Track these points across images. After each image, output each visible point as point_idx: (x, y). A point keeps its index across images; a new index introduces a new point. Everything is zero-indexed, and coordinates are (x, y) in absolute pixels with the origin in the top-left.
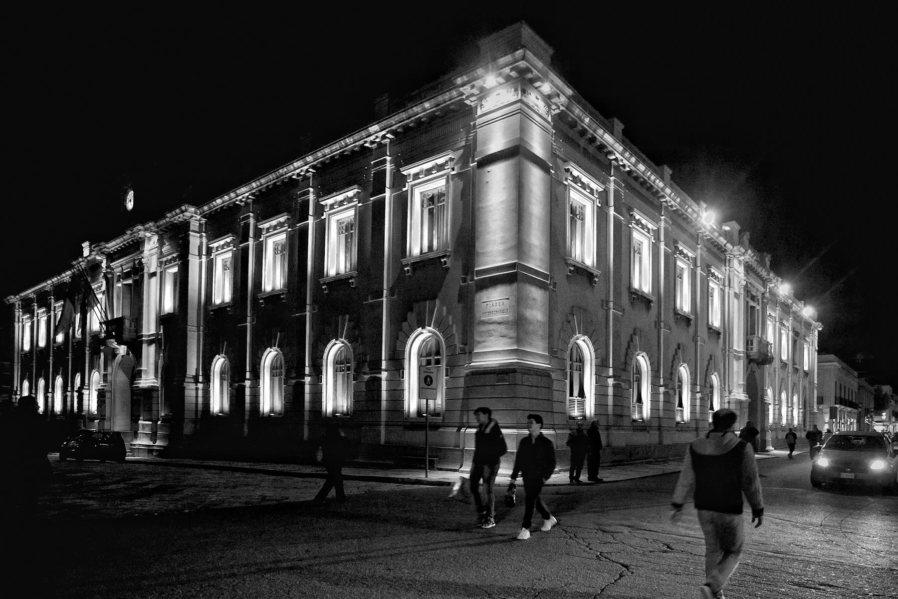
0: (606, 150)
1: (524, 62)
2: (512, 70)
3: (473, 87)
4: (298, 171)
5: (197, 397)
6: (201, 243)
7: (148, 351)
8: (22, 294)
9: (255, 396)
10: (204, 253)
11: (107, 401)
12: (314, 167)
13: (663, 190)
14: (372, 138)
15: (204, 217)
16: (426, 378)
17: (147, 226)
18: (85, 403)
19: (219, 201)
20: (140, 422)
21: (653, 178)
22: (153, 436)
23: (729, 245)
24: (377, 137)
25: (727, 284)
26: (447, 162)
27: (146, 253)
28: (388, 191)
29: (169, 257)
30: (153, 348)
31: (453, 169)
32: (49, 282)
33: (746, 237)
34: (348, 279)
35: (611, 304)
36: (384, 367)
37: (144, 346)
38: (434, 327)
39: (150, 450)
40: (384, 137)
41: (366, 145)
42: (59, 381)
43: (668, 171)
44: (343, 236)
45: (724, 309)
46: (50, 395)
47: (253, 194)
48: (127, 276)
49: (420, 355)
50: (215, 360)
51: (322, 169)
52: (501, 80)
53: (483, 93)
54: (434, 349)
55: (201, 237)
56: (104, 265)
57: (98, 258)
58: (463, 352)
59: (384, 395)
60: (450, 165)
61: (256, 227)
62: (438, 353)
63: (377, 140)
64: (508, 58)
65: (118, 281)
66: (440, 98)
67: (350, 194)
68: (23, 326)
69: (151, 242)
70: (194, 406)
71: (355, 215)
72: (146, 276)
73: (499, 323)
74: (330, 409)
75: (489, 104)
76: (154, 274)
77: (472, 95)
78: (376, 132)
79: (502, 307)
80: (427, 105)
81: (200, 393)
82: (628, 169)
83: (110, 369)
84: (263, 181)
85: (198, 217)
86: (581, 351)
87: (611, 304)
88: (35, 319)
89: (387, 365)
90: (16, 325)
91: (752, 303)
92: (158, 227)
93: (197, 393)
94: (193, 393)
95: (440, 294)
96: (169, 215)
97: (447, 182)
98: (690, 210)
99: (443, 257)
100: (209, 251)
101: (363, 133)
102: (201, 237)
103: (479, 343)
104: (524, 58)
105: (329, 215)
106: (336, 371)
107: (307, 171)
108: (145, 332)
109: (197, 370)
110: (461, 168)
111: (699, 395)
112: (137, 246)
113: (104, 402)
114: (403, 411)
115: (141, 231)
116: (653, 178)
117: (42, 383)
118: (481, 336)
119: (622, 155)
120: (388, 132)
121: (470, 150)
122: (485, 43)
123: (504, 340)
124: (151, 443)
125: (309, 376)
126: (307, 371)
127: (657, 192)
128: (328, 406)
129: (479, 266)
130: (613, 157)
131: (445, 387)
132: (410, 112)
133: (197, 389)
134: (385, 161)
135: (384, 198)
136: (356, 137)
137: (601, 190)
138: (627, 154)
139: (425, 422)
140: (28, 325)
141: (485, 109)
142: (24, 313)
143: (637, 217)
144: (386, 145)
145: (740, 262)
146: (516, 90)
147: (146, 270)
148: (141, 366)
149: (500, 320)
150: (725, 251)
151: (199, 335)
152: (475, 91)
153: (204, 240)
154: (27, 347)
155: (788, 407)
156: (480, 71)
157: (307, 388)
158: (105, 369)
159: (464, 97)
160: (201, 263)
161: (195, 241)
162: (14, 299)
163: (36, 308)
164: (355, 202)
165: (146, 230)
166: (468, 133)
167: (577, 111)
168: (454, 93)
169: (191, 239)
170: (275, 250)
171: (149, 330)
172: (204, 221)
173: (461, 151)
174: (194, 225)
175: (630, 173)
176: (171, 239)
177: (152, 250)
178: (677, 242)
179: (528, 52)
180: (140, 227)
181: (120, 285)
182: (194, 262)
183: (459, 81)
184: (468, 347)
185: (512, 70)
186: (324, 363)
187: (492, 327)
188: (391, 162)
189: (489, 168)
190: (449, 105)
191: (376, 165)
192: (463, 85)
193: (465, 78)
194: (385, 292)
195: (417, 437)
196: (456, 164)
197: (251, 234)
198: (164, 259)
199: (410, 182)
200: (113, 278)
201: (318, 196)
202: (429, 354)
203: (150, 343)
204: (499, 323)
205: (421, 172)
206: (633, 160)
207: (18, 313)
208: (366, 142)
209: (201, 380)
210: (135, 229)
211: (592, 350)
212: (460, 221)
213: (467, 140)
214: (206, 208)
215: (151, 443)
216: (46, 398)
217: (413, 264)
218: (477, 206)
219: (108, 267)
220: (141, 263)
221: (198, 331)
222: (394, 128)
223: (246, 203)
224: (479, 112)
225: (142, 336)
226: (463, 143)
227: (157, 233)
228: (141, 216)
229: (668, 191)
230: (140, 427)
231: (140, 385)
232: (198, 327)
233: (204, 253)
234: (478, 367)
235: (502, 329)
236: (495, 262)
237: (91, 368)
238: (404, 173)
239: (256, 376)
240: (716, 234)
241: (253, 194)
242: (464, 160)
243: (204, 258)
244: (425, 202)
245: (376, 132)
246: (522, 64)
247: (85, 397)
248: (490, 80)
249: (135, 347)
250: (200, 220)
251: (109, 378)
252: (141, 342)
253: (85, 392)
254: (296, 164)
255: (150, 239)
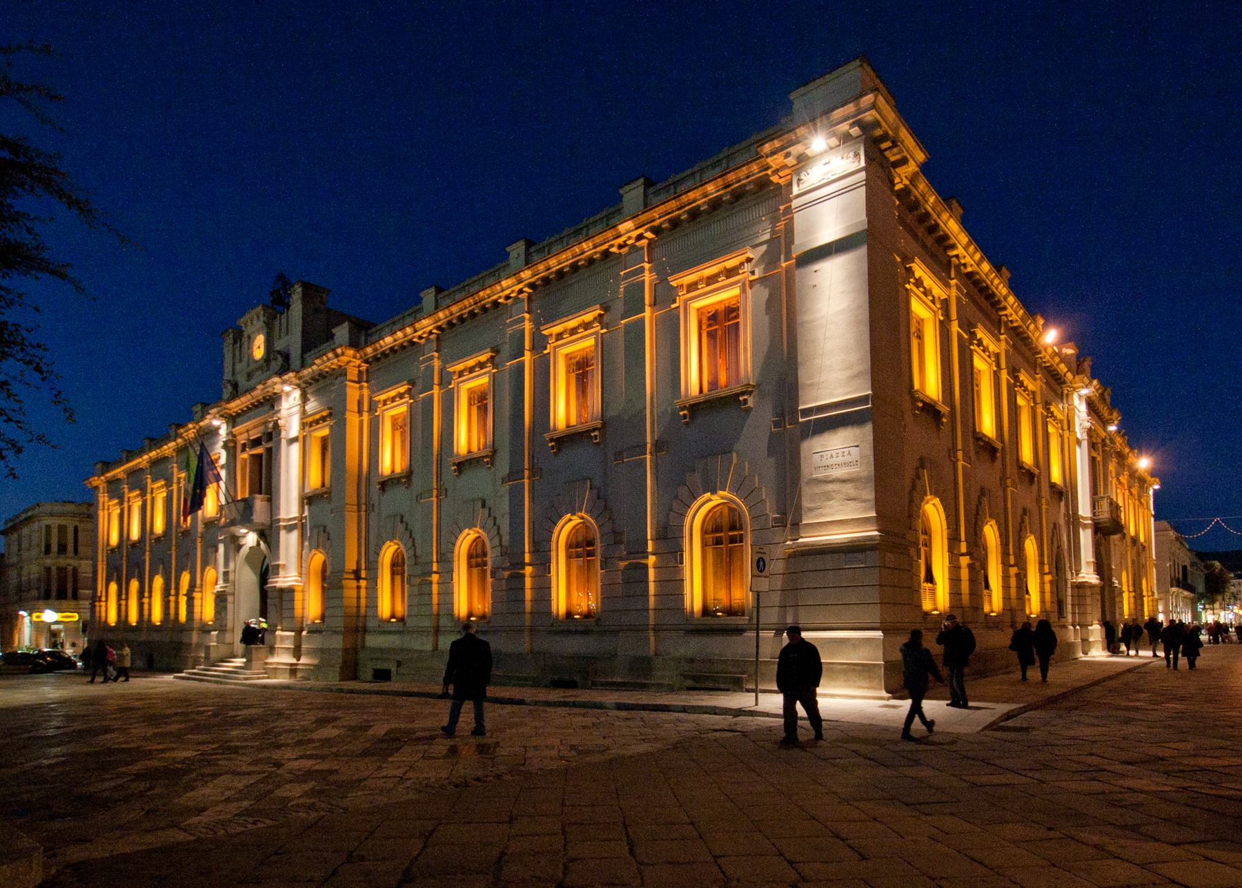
0: (946, 243)
1: (873, 112)
2: (852, 125)
3: (788, 155)
4: (507, 292)
5: (358, 598)
6: (362, 396)
7: (287, 539)
8: (108, 475)
9: (543, 591)
10: (366, 407)
11: (230, 606)
12: (532, 286)
13: (1005, 298)
14: (620, 241)
15: (366, 361)
16: (758, 562)
17: (286, 377)
18: (197, 609)
19: (388, 340)
20: (278, 633)
21: (996, 281)
22: (297, 652)
23: (1069, 375)
24: (630, 238)
25: (1066, 427)
26: (742, 264)
27: (284, 413)
28: (648, 309)
29: (317, 417)
30: (294, 536)
31: (753, 273)
32: (146, 457)
33: (1087, 365)
34: (589, 431)
35: (960, 454)
36: (650, 549)
37: (283, 533)
38: (586, 512)
39: (293, 670)
40: (640, 237)
41: (614, 250)
42: (158, 582)
43: (1006, 273)
44: (573, 376)
45: (1071, 464)
46: (123, 602)
47: (439, 328)
48: (256, 442)
49: (704, 532)
50: (384, 548)
51: (543, 286)
52: (834, 141)
53: (803, 161)
54: (479, 551)
55: (361, 388)
56: (223, 431)
57: (216, 423)
58: (781, 523)
59: (528, 594)
60: (747, 267)
61: (442, 370)
62: (485, 555)
63: (629, 242)
64: (850, 108)
65: (243, 450)
66: (731, 177)
67: (588, 317)
68: (109, 515)
69: (291, 399)
70: (354, 610)
71: (596, 345)
72: (284, 442)
73: (844, 481)
74: (562, 609)
75: (813, 176)
76: (295, 440)
77: (785, 167)
78: (628, 232)
79: (847, 459)
80: (710, 188)
81: (363, 593)
82: (970, 269)
83: (232, 565)
84: (454, 309)
85: (358, 362)
86: (928, 519)
87: (960, 454)
88: (126, 505)
89: (531, 559)
90: (101, 513)
91: (1094, 454)
92: (300, 379)
93: (358, 593)
94: (354, 593)
95: (738, 446)
96: (318, 361)
97: (743, 291)
98: (1032, 326)
99: (743, 393)
100: (372, 409)
101: (609, 234)
102: (361, 388)
103: (811, 510)
104: (874, 106)
105: (555, 348)
106: (569, 557)
107: (521, 291)
108: (283, 515)
109: (358, 562)
110: (766, 270)
111: (1048, 578)
112: (272, 402)
113: (225, 608)
114: (683, 609)
115: (278, 385)
116: (996, 281)
117: (134, 585)
118: (813, 500)
119: (966, 253)
120: (646, 230)
121: (783, 240)
122: (818, 91)
123: (852, 504)
124: (294, 661)
125: (529, 565)
126: (527, 558)
127: (999, 302)
128: (560, 603)
129: (804, 403)
130: (955, 253)
131: (600, 584)
132: (684, 198)
133: (359, 588)
134: (642, 270)
135: (643, 319)
136: (598, 240)
137: (944, 296)
138: (972, 249)
139: (718, 623)
140: (116, 512)
141: (805, 186)
142: (111, 498)
143: (980, 335)
144: (642, 248)
145: (1080, 396)
146: (857, 155)
147: (283, 434)
148: (278, 558)
149: (846, 477)
150: (1064, 382)
151: (359, 518)
152: (791, 161)
153: (366, 392)
154: (114, 539)
155: (1005, 564)
156: (801, 131)
157: (528, 582)
158: (226, 564)
159: (769, 172)
160: (361, 422)
161: (353, 393)
162: (99, 481)
163: (126, 490)
164: (597, 327)
165: (284, 382)
166: (775, 220)
167: (922, 185)
168: (755, 168)
169: (349, 391)
170: (470, 399)
171: (288, 512)
172: (364, 367)
173: (764, 247)
174: (352, 373)
175: (970, 275)
176: (317, 393)
177: (292, 408)
178: (1019, 371)
179: (880, 97)
180: (276, 379)
181: (245, 456)
182: (352, 419)
183: (767, 148)
184: (790, 514)
185: (852, 125)
186: (456, 559)
187: (830, 487)
188: (650, 271)
189: (816, 267)
190: (745, 185)
191: (627, 276)
192: (773, 153)
193: (777, 144)
194: (649, 446)
195: (715, 646)
196: (756, 265)
197: (436, 381)
198: (310, 419)
199: (683, 296)
200: (235, 447)
201: (538, 324)
202: (718, 529)
203: (290, 529)
204: (844, 481)
205: (701, 280)
206: (978, 256)
207: (103, 498)
208: (612, 246)
209: (363, 575)
210: (269, 382)
211: (943, 517)
212: (766, 341)
213: (773, 232)
214: (369, 350)
215: (294, 661)
216: (119, 606)
217: (692, 406)
218: (799, 319)
219: (229, 433)
220: (276, 426)
221: (359, 511)
222: (656, 223)
223: (427, 339)
224: (796, 190)
225: (279, 520)
226: (767, 237)
227: (298, 386)
228: (280, 362)
229: (1011, 299)
230: (278, 640)
231: (278, 585)
232: (359, 505)
233: (366, 407)
234: (805, 545)
235: (849, 489)
236: (833, 396)
237: (205, 564)
238: (674, 284)
239: (177, 595)
240: (1057, 359)
241: (439, 328)
242: (770, 259)
243: (366, 417)
244: (704, 321)
245: (628, 232)
246: (869, 116)
247: (197, 602)
248: (818, 143)
249: (268, 534)
250: (359, 366)
251: (231, 577)
252: (278, 529)
253: (197, 595)
254: (504, 283)
255: (288, 394)
